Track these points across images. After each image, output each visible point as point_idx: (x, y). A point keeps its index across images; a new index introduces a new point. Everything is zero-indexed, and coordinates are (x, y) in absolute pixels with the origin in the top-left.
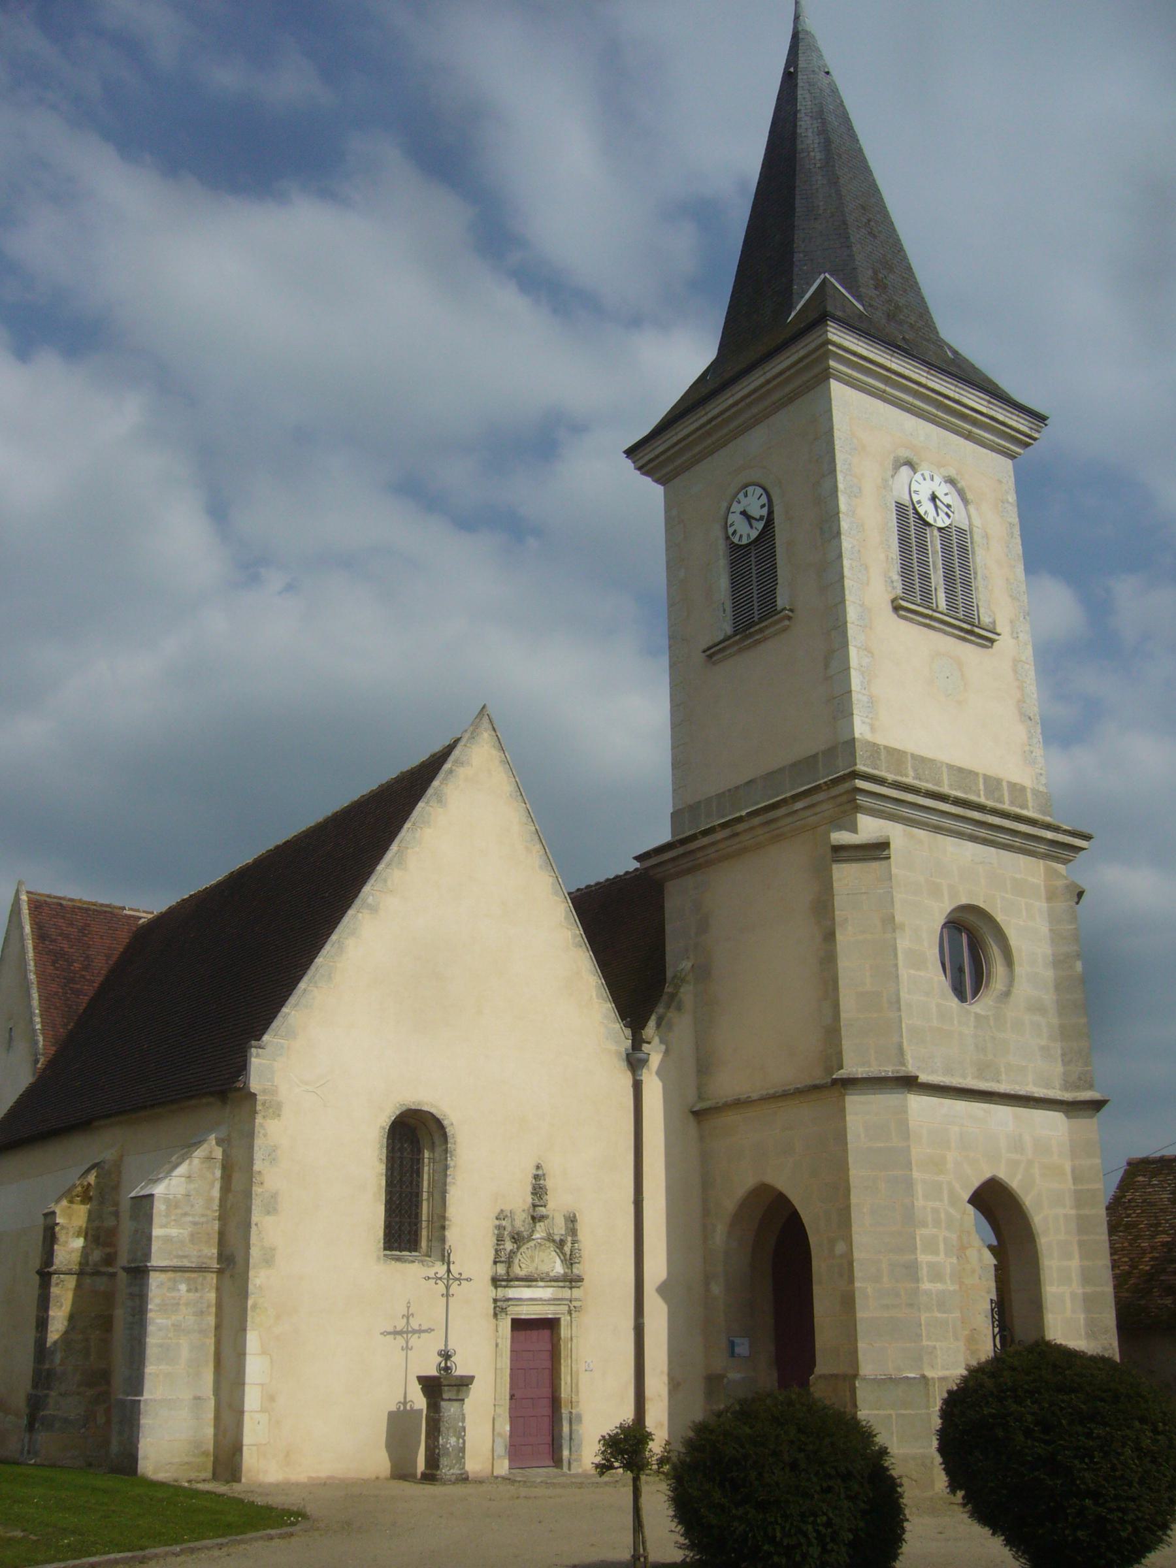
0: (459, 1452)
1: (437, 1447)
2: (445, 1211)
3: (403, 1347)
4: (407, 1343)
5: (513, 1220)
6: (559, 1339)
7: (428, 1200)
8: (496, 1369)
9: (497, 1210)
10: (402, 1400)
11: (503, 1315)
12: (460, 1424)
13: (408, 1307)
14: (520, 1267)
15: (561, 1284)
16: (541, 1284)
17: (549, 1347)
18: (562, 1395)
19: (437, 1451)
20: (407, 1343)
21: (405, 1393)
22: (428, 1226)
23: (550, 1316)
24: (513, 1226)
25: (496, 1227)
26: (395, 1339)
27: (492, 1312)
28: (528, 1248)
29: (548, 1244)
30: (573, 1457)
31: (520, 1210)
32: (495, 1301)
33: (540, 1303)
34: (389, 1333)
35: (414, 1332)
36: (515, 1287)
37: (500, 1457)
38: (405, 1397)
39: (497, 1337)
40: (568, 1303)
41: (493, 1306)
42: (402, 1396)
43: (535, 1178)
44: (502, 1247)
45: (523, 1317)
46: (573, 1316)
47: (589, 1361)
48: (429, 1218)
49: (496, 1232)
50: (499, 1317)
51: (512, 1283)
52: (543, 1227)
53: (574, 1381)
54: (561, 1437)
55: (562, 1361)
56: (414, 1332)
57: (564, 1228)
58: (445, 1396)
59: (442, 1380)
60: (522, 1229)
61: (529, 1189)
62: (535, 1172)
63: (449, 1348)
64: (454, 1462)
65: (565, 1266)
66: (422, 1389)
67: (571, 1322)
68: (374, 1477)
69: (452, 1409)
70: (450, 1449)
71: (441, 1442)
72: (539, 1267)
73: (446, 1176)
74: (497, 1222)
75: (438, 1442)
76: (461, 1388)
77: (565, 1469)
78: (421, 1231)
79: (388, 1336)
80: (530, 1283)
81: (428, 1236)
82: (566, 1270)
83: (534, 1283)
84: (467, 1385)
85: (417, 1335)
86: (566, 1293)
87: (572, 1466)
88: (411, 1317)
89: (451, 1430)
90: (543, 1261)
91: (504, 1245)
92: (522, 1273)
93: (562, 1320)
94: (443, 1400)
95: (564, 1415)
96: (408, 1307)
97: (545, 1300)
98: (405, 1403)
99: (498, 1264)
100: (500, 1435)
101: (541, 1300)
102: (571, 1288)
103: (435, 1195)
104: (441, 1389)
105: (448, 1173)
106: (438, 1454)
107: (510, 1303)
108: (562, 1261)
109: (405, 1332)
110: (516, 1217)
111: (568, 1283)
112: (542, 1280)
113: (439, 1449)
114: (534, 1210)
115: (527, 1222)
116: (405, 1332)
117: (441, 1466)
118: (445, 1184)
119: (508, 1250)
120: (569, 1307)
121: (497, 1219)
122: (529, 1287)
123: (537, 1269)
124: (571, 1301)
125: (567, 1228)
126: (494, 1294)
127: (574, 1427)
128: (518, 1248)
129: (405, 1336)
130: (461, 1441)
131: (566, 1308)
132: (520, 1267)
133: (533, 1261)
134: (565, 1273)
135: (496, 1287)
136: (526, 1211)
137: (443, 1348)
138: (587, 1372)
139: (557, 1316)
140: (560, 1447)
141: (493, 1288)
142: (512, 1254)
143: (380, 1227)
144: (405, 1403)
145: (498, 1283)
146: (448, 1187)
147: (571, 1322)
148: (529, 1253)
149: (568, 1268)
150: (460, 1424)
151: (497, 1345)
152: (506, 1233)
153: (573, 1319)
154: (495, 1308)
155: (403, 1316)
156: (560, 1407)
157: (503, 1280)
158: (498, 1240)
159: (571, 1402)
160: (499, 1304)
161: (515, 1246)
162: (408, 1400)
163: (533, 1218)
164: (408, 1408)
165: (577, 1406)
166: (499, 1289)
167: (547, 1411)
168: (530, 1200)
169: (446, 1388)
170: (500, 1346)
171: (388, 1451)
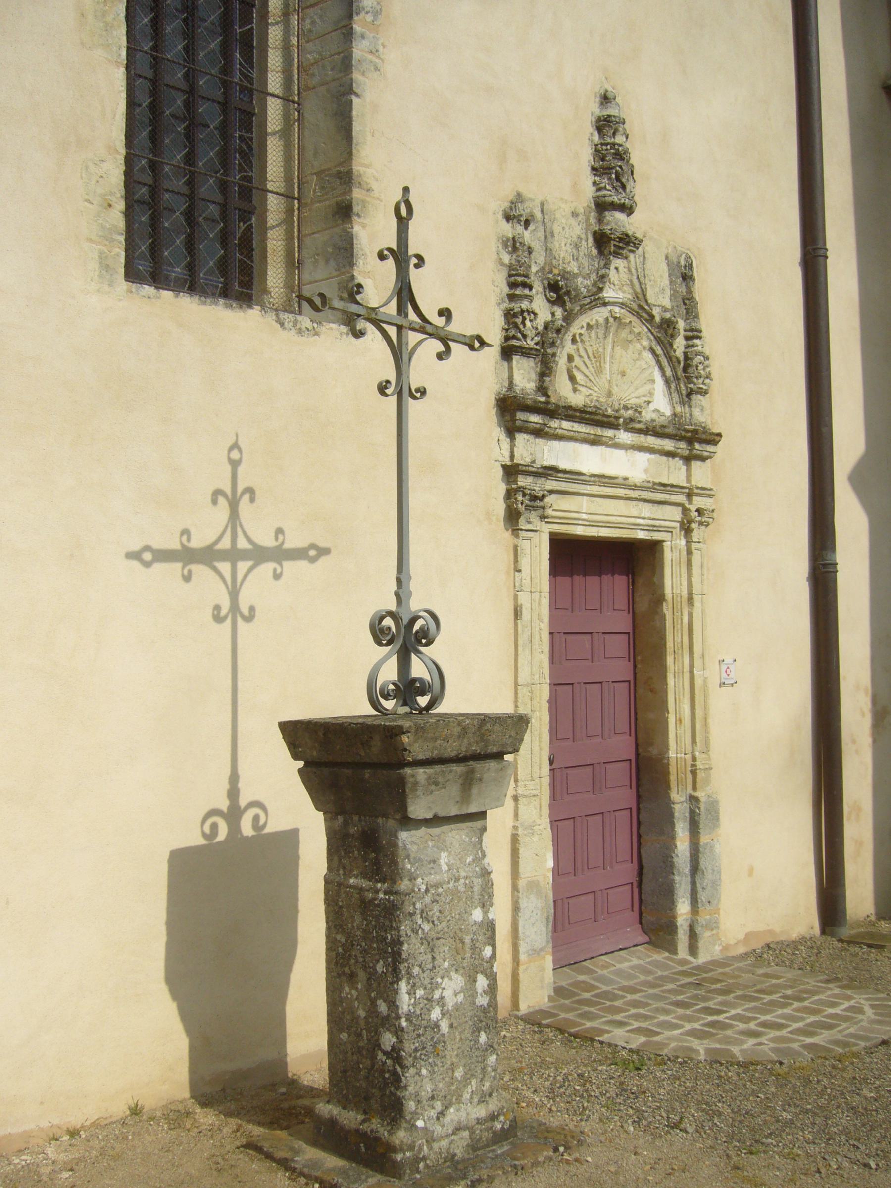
0: (477, 1030)
1: (390, 1021)
2: (349, 155)
3: (217, 608)
4: (234, 594)
5: (549, 235)
6: (659, 599)
7: (285, 133)
8: (516, 684)
9: (507, 192)
10: (224, 804)
11: (534, 516)
12: (477, 915)
13: (235, 465)
14: (572, 378)
15: (668, 445)
16: (624, 437)
17: (623, 623)
18: (672, 754)
19: (388, 1040)
20: (234, 594)
21: (234, 778)
22: (288, 220)
23: (641, 535)
24: (548, 250)
25: (505, 246)
26: (187, 578)
27: (500, 508)
28: (589, 327)
29: (639, 327)
30: (703, 918)
31: (567, 209)
32: (511, 471)
33: (621, 492)
34: (164, 556)
35: (260, 555)
36: (560, 438)
37: (536, 953)
38: (233, 793)
39: (516, 591)
40: (681, 499)
41: (502, 488)
42: (224, 785)
43: (600, 129)
44: (525, 305)
45: (580, 531)
46: (695, 536)
47: (729, 660)
48: (288, 179)
49: (506, 259)
50: (522, 524)
51: (554, 424)
52: (624, 275)
53: (699, 713)
54: (667, 864)
55: (670, 660)
56: (260, 555)
57: (668, 292)
58: (418, 809)
59: (405, 739)
60: (573, 267)
61: (586, 156)
62: (598, 112)
63: (416, 604)
64: (459, 1073)
65: (675, 395)
66: (300, 771)
67: (689, 553)
68: (120, 1109)
69: (444, 858)
70: (444, 1026)
71: (405, 1002)
72: (615, 390)
73: (348, 34)
74: (508, 229)
75: (393, 1004)
76: (477, 765)
77: (682, 952)
78: (264, 239)
79: (158, 567)
80: (599, 431)
81: (289, 253)
82: (678, 409)
83: (610, 433)
84: (499, 756)
85: (268, 567)
86: (675, 472)
87: (701, 944)
88: (244, 503)
89: (444, 948)
90: (623, 374)
91: (530, 298)
92: (577, 400)
93: (667, 545)
94: (407, 822)
95: (677, 807)
96: (235, 465)
97: (635, 487)
98: (233, 814)
99: (516, 359)
100: (533, 885)
101: (625, 483)
102: (687, 460)
103: (308, 116)
104: (402, 781)
105: (357, 28)
106: (395, 1054)
107: (551, 484)
108: (667, 382)
109: (225, 556)
110: (557, 229)
111: (683, 445)
112: (630, 425)
113: (398, 1031)
114: (600, 221)
115: (583, 250)
116: (225, 556)
117: (411, 1105)
118: (346, 64)
119: (540, 323)
120: (685, 511)
121: (508, 218)
122: (595, 442)
123: (609, 394)
124: (689, 496)
125: (673, 296)
126: (507, 454)
127: (704, 839)
128: (569, 318)
129: (225, 567)
130: (482, 982)
131: (675, 514)
132: (572, 378)
133: (599, 371)
134: (675, 415)
135: (512, 430)
136: (581, 218)
137: (392, 606)
138: (724, 689)
139: (657, 536)
140: (668, 893)
141: (499, 433)
142: (552, 335)
143: (111, 149)
144: (233, 814)
145: (520, 416)
146: (356, 75)
147: (689, 553)
148: (592, 343)
149: (682, 403)
150: (477, 915)
151: (517, 613)
152: (534, 269)
153: (694, 546)
154: (510, 495)
155: (217, 493)
156: (668, 787)
157: (534, 409)
158: (513, 285)
159: (694, 773)
160: (523, 481)
161: (559, 312)
162: (243, 803)
163: (601, 240)
164: (247, 829)
165: (707, 781)
166: (521, 438)
167: (625, 796)
168: (588, 191)
169: (421, 773)
170: (526, 615)
171: (175, 994)
